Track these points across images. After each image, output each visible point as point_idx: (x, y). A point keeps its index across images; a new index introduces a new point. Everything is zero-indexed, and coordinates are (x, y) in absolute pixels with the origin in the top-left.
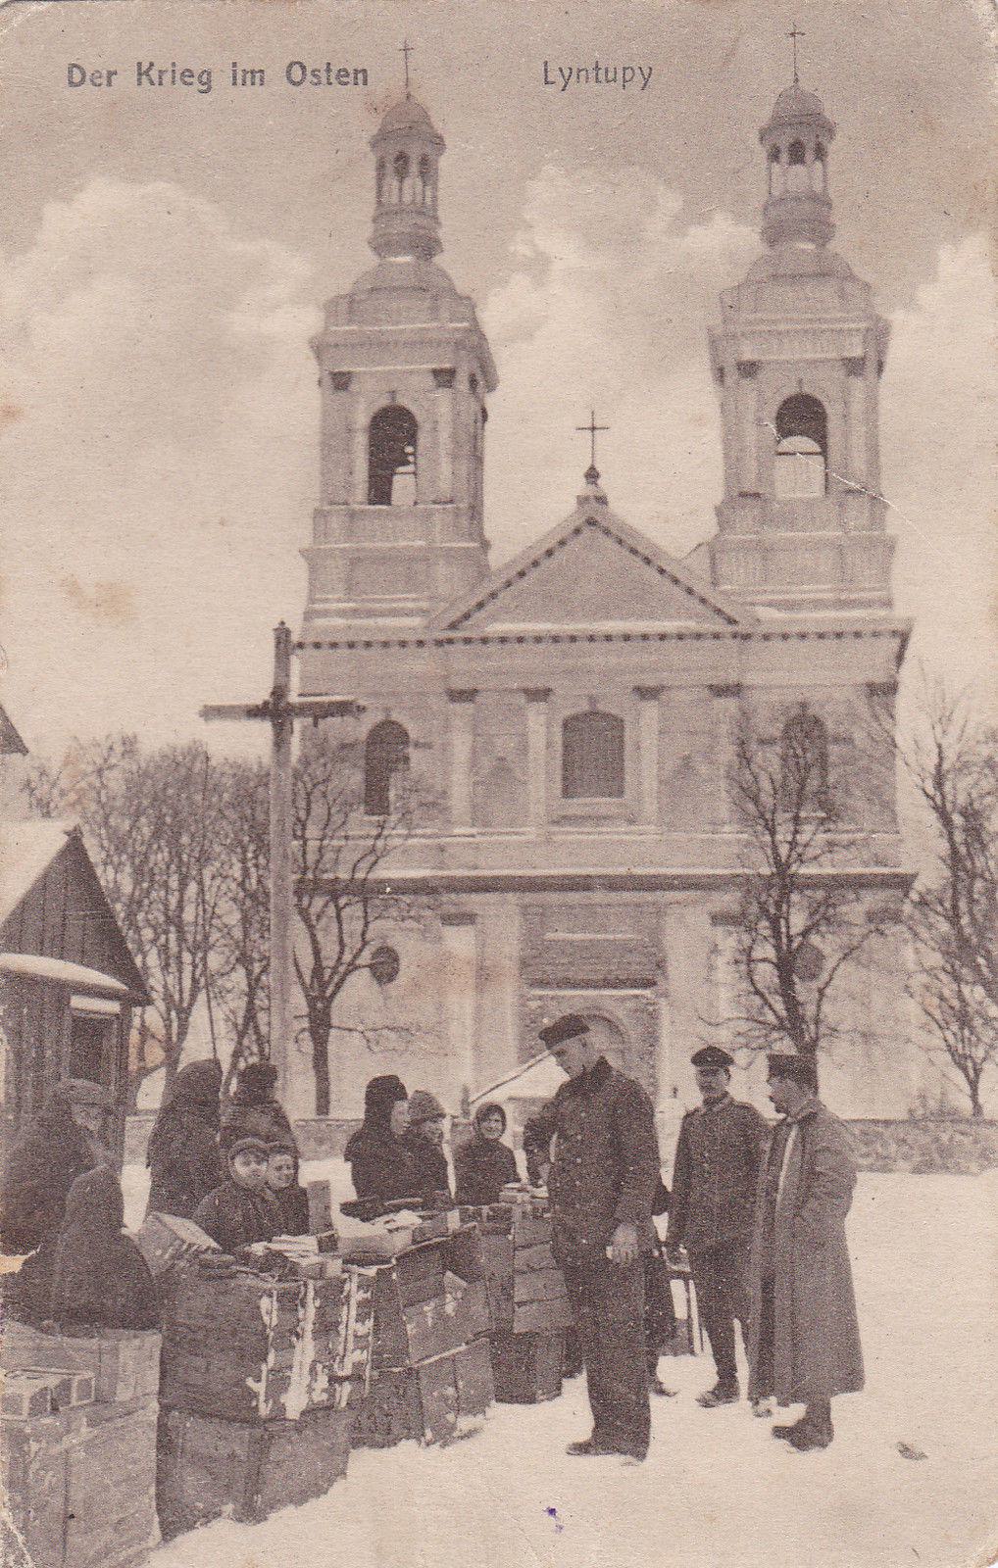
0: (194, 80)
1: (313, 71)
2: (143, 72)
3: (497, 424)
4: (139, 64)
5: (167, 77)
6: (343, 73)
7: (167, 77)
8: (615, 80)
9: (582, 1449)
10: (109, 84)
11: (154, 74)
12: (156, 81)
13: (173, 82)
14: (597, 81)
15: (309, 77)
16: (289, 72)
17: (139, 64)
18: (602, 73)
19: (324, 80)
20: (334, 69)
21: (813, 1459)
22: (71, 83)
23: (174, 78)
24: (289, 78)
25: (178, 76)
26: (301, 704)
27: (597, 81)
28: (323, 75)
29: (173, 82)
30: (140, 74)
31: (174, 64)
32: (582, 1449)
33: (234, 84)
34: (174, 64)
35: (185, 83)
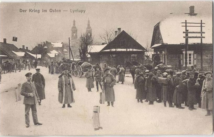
0: (37, 11)
1: (53, 10)
2: (30, 10)
3: (20, 14)
4: (30, 9)
5: (33, 11)
6: (36, 10)
7: (33, 11)
8: (44, 10)
9: (206, 115)
10: (26, 11)
11: (32, 11)
12: (32, 11)
13: (34, 12)
14: (55, 12)
15: (53, 11)
16: (50, 10)
17: (30, 9)
18: (78, 11)
19: (55, 11)
20: (56, 10)
21: (103, 128)
22: (20, 12)
23: (34, 11)
24: (50, 12)
25: (56, 11)
26: (185, 104)
27: (55, 12)
28: (55, 11)
29: (34, 12)
30: (30, 11)
31: (34, 9)
32: (206, 115)
33: (43, 12)
34: (55, 9)
35: (23, 12)
